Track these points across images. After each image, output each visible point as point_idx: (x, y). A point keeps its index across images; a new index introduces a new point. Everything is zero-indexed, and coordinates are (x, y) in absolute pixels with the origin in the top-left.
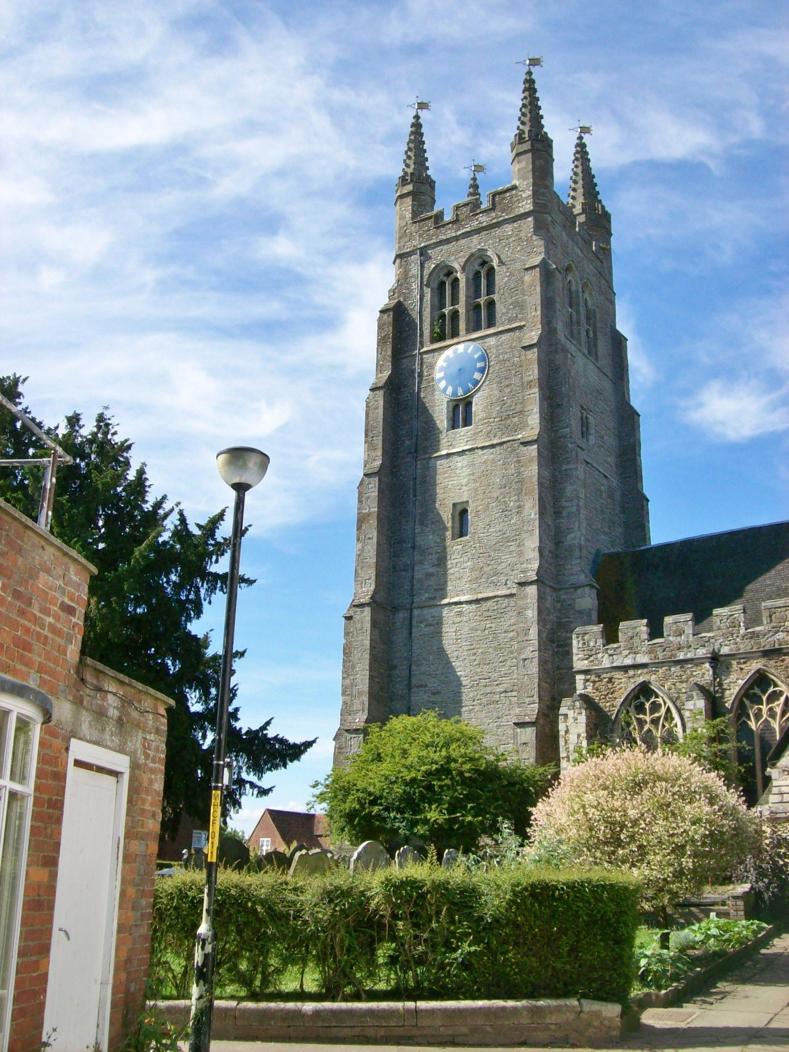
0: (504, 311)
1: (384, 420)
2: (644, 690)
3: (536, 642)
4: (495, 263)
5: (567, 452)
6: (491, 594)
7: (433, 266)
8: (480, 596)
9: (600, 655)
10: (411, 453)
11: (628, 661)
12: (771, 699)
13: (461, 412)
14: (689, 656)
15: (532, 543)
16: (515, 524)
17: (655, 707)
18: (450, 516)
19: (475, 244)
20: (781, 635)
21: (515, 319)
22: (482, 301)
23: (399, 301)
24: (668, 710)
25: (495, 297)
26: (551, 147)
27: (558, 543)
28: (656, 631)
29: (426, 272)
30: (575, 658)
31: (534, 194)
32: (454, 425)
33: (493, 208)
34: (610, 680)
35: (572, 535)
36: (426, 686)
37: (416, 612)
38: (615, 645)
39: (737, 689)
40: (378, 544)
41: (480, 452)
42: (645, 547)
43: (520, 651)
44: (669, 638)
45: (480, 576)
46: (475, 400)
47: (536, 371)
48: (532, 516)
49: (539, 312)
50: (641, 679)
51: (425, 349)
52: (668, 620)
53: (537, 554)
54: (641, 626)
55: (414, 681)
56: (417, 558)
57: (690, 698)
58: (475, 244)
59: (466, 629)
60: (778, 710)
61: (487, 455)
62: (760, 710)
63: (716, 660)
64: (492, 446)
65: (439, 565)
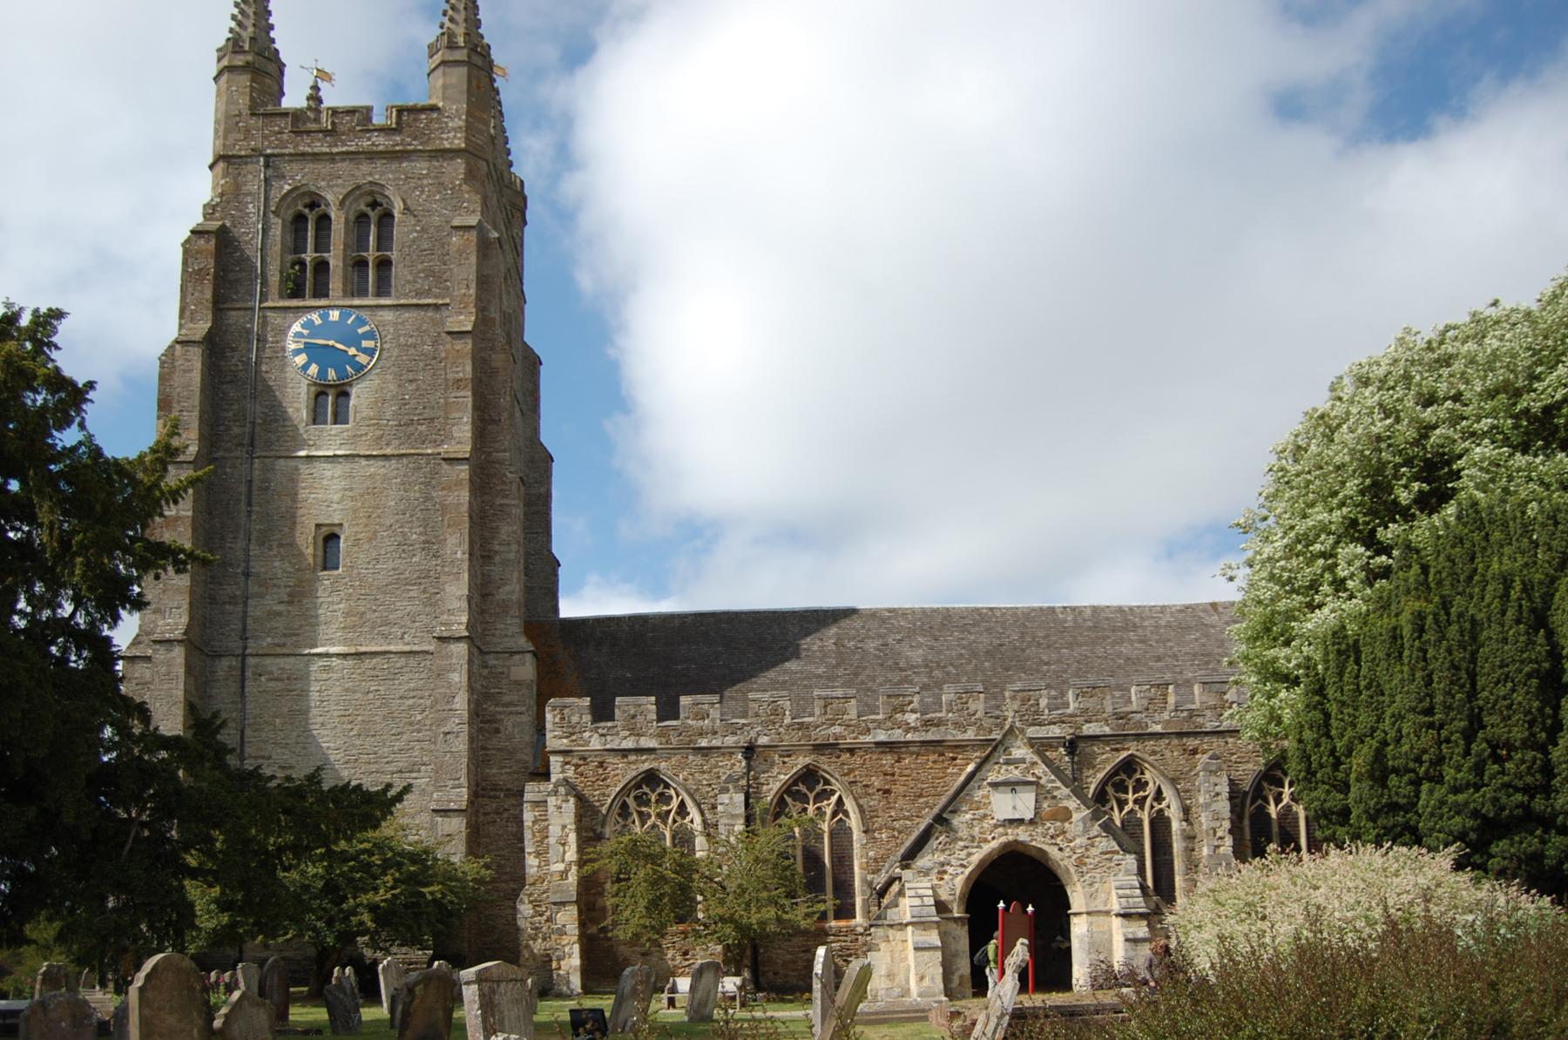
0: (410, 278)
1: (202, 391)
2: (651, 778)
3: (466, 714)
4: (398, 208)
5: (504, 483)
6: (378, 649)
7: (287, 187)
8: (363, 649)
9: (587, 735)
10: (242, 445)
11: (629, 744)
12: (818, 798)
13: (331, 398)
14: (715, 743)
15: (457, 591)
16: (419, 564)
17: (664, 799)
18: (310, 539)
19: (366, 173)
20: (837, 729)
21: (428, 293)
22: (371, 255)
23: (224, 226)
24: (682, 805)
25: (394, 255)
26: (282, 73)
27: (485, 596)
28: (668, 710)
29: (276, 196)
30: (549, 735)
31: (467, 128)
32: (317, 417)
33: (397, 130)
34: (601, 764)
35: (507, 588)
36: (270, 758)
37: (251, 661)
38: (610, 724)
39: (778, 785)
41: (364, 462)
43: (441, 722)
44: (687, 720)
45: (356, 622)
46: (354, 391)
47: (469, 368)
48: (459, 555)
49: (472, 291)
50: (646, 766)
51: (269, 304)
52: (685, 701)
53: (465, 605)
54: (649, 703)
56: (254, 589)
57: (725, 790)
58: (366, 173)
59: (338, 689)
60: (829, 811)
61: (375, 468)
63: (750, 751)
64: (385, 457)
65: (290, 603)
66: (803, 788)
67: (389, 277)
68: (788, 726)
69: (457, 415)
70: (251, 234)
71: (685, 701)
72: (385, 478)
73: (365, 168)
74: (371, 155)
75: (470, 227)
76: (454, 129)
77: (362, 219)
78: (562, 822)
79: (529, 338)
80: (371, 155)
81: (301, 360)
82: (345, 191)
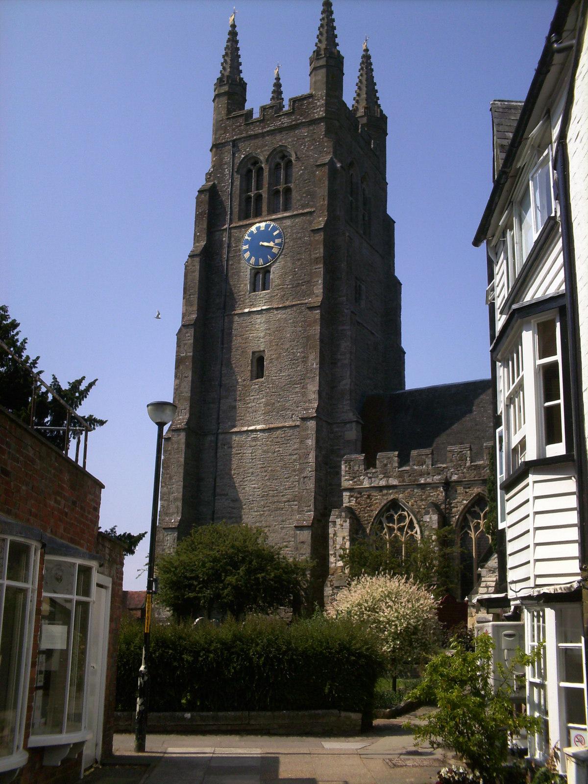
2: (394, 505)
4: (293, 158)
7: (243, 156)
9: (362, 478)
11: (383, 483)
14: (429, 480)
22: (281, 188)
23: (214, 183)
24: (411, 522)
28: (404, 460)
29: (237, 161)
30: (343, 479)
34: (369, 497)
35: (344, 382)
36: (227, 495)
40: (193, 382)
42: (401, 391)
45: (272, 409)
47: (322, 250)
48: (314, 366)
49: (326, 202)
50: (392, 497)
52: (414, 453)
53: (316, 396)
55: (218, 490)
58: (280, 140)
61: (280, 315)
62: (479, 523)
63: (448, 485)
66: (477, 509)
67: (290, 198)
68: (469, 468)
69: (316, 280)
70: (225, 187)
71: (414, 453)
72: (286, 320)
73: (278, 137)
74: (281, 130)
75: (324, 164)
76: (319, 106)
77: (278, 166)
78: (342, 535)
79: (389, 212)
80: (281, 130)
81: (247, 255)
82: (268, 153)
